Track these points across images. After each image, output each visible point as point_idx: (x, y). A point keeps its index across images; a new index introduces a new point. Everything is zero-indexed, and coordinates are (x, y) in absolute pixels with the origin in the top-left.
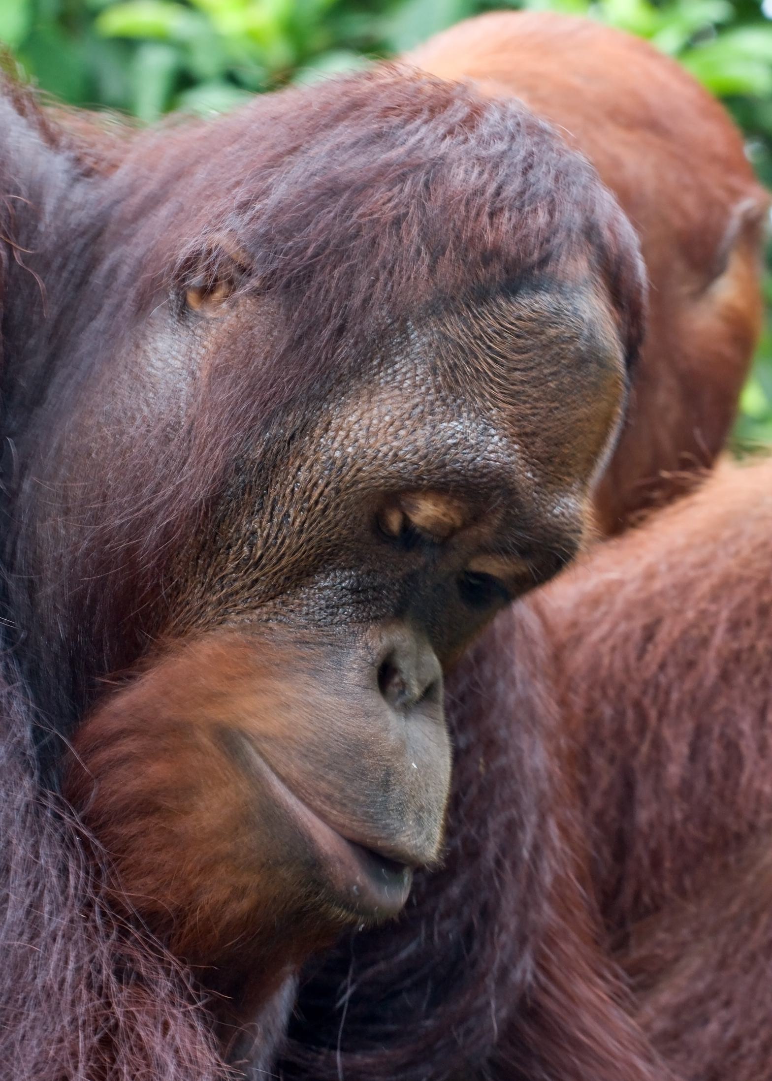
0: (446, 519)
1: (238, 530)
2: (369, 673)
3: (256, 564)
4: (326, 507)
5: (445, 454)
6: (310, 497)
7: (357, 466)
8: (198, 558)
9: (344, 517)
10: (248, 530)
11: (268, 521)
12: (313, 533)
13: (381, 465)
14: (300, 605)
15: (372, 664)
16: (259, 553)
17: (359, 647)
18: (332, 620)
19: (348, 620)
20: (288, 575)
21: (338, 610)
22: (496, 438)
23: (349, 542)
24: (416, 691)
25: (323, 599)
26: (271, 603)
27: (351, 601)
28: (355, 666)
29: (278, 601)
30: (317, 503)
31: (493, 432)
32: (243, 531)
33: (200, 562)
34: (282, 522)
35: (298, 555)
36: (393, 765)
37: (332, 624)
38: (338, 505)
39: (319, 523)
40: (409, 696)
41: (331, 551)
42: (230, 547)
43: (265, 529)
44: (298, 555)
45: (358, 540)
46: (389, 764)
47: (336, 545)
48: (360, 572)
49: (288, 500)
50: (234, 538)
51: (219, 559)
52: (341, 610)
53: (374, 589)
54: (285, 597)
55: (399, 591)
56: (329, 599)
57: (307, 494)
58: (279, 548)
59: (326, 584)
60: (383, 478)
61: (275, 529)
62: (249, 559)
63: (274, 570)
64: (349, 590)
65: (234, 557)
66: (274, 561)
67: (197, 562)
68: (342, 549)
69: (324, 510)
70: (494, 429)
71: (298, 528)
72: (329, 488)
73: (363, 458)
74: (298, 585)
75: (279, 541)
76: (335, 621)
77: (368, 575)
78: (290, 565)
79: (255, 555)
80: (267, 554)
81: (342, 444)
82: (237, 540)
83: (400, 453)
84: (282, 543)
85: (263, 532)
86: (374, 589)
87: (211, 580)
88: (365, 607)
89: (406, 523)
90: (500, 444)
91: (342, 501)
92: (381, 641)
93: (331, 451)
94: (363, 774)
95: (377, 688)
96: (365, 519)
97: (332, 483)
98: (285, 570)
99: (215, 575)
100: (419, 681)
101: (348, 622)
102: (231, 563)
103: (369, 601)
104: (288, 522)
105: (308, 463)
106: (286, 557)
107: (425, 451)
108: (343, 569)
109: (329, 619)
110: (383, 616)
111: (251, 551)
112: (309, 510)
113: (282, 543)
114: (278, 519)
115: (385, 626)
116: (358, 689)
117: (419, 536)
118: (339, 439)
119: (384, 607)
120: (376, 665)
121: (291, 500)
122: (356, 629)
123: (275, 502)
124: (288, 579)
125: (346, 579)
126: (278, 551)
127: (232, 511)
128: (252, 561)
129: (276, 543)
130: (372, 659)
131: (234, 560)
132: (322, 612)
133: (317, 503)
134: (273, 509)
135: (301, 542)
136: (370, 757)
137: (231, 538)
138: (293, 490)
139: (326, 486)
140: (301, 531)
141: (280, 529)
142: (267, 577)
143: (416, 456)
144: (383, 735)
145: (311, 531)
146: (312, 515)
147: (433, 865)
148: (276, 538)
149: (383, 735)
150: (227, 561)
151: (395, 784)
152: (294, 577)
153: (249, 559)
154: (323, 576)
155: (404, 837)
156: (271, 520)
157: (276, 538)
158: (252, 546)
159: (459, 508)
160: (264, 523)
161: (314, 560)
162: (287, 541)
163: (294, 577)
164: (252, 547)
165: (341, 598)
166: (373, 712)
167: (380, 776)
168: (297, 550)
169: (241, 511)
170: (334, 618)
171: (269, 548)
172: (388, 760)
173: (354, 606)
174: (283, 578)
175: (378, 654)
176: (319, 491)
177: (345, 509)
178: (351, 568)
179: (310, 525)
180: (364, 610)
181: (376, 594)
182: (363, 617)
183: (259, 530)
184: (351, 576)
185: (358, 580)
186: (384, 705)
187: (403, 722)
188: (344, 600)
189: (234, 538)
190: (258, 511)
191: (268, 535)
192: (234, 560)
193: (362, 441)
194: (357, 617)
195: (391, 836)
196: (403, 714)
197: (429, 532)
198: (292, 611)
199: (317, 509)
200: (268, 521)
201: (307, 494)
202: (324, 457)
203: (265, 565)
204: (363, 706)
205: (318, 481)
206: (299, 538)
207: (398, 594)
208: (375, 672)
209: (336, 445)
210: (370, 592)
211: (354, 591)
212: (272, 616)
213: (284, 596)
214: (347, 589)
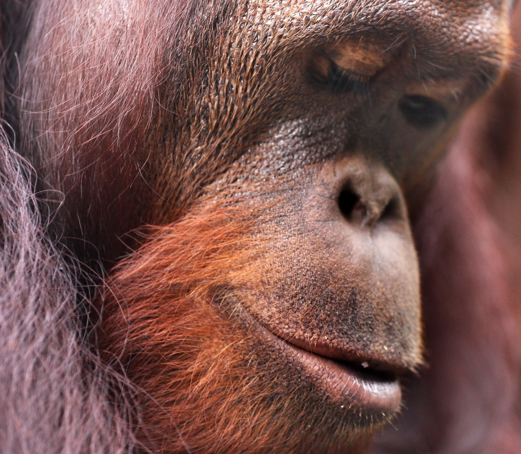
0: (367, 62)
1: (192, 108)
2: (328, 207)
3: (215, 132)
4: (261, 72)
5: (350, 11)
6: (245, 67)
7: (278, 34)
8: (164, 140)
9: (279, 76)
10: (200, 107)
11: (216, 95)
12: (256, 96)
13: (297, 30)
14: (261, 160)
15: (330, 197)
16: (215, 122)
17: (316, 185)
18: (290, 167)
19: (304, 163)
20: (245, 135)
21: (293, 157)
23: (289, 96)
24: (376, 210)
25: (279, 149)
26: (235, 164)
27: (303, 146)
28: (314, 204)
30: (252, 71)
32: (197, 108)
33: (167, 143)
34: (227, 93)
35: (248, 118)
36: (358, 286)
37: (290, 170)
38: (271, 68)
39: (259, 86)
40: (372, 216)
41: (276, 107)
42: (189, 123)
43: (214, 102)
44: (248, 118)
48: (307, 120)
49: (227, 73)
50: (191, 115)
51: (183, 137)
52: (296, 156)
53: (322, 131)
55: (345, 127)
56: (284, 148)
57: (242, 65)
58: (230, 115)
59: (280, 136)
60: (302, 39)
62: (207, 129)
63: (231, 135)
64: (300, 136)
65: (195, 131)
66: (229, 127)
67: (165, 144)
68: (285, 104)
71: (242, 95)
72: (259, 56)
73: (282, 27)
75: (229, 109)
76: (292, 166)
77: (314, 120)
78: (243, 127)
79: (211, 124)
80: (221, 122)
81: (262, 19)
82: (193, 116)
83: (311, 17)
84: (232, 109)
85: (213, 104)
86: (322, 131)
87: (180, 157)
88: (317, 149)
89: (334, 67)
91: (273, 64)
92: (335, 175)
93: (253, 27)
94: (332, 299)
96: (298, 74)
97: (261, 52)
98: (241, 131)
99: (183, 152)
100: (377, 201)
101: (304, 166)
102: (193, 137)
103: (320, 143)
104: (232, 92)
106: (238, 121)
107: (333, 12)
108: (292, 120)
109: (287, 166)
110: (334, 153)
111: (207, 122)
113: (232, 109)
114: (223, 90)
115: (336, 161)
117: (346, 78)
118: (258, 15)
119: (335, 145)
120: (333, 197)
121: (230, 72)
122: (311, 170)
123: (217, 77)
124: (245, 139)
125: (295, 128)
126: (230, 118)
127: (182, 93)
128: (210, 131)
129: (227, 110)
130: (329, 193)
131: (195, 133)
132: (280, 162)
133: (252, 71)
134: (217, 83)
135: (247, 106)
136: (336, 282)
137: (188, 116)
138: (229, 65)
139: (257, 55)
140: (245, 97)
142: (227, 142)
143: (325, 17)
145: (254, 95)
146: (251, 81)
147: (419, 367)
148: (226, 107)
150: (190, 136)
151: (362, 302)
152: (251, 136)
153: (207, 129)
154: (275, 129)
156: (218, 93)
157: (226, 107)
158: (206, 118)
160: (212, 97)
161: (263, 118)
162: (236, 108)
163: (251, 136)
164: (208, 119)
165: (295, 145)
166: (334, 242)
167: (346, 297)
168: (246, 113)
169: (190, 91)
170: (291, 164)
171: (221, 117)
172: (352, 282)
173: (307, 150)
174: (241, 139)
175: (334, 187)
176: (252, 60)
177: (277, 70)
178: (298, 118)
179: (252, 90)
180: (316, 152)
181: (325, 135)
182: (316, 158)
183: (210, 105)
184: (299, 125)
185: (306, 127)
188: (297, 146)
189: (191, 115)
190: (205, 88)
191: (219, 107)
192: (195, 133)
193: (278, 13)
194: (311, 159)
196: (369, 233)
197: (354, 73)
198: (255, 167)
199: (254, 75)
200: (216, 95)
201: (242, 65)
202: (249, 32)
203: (222, 131)
204: (324, 239)
205: (248, 53)
206: (245, 103)
208: (334, 203)
209: (257, 21)
210: (320, 134)
212: (238, 176)
213: (246, 155)
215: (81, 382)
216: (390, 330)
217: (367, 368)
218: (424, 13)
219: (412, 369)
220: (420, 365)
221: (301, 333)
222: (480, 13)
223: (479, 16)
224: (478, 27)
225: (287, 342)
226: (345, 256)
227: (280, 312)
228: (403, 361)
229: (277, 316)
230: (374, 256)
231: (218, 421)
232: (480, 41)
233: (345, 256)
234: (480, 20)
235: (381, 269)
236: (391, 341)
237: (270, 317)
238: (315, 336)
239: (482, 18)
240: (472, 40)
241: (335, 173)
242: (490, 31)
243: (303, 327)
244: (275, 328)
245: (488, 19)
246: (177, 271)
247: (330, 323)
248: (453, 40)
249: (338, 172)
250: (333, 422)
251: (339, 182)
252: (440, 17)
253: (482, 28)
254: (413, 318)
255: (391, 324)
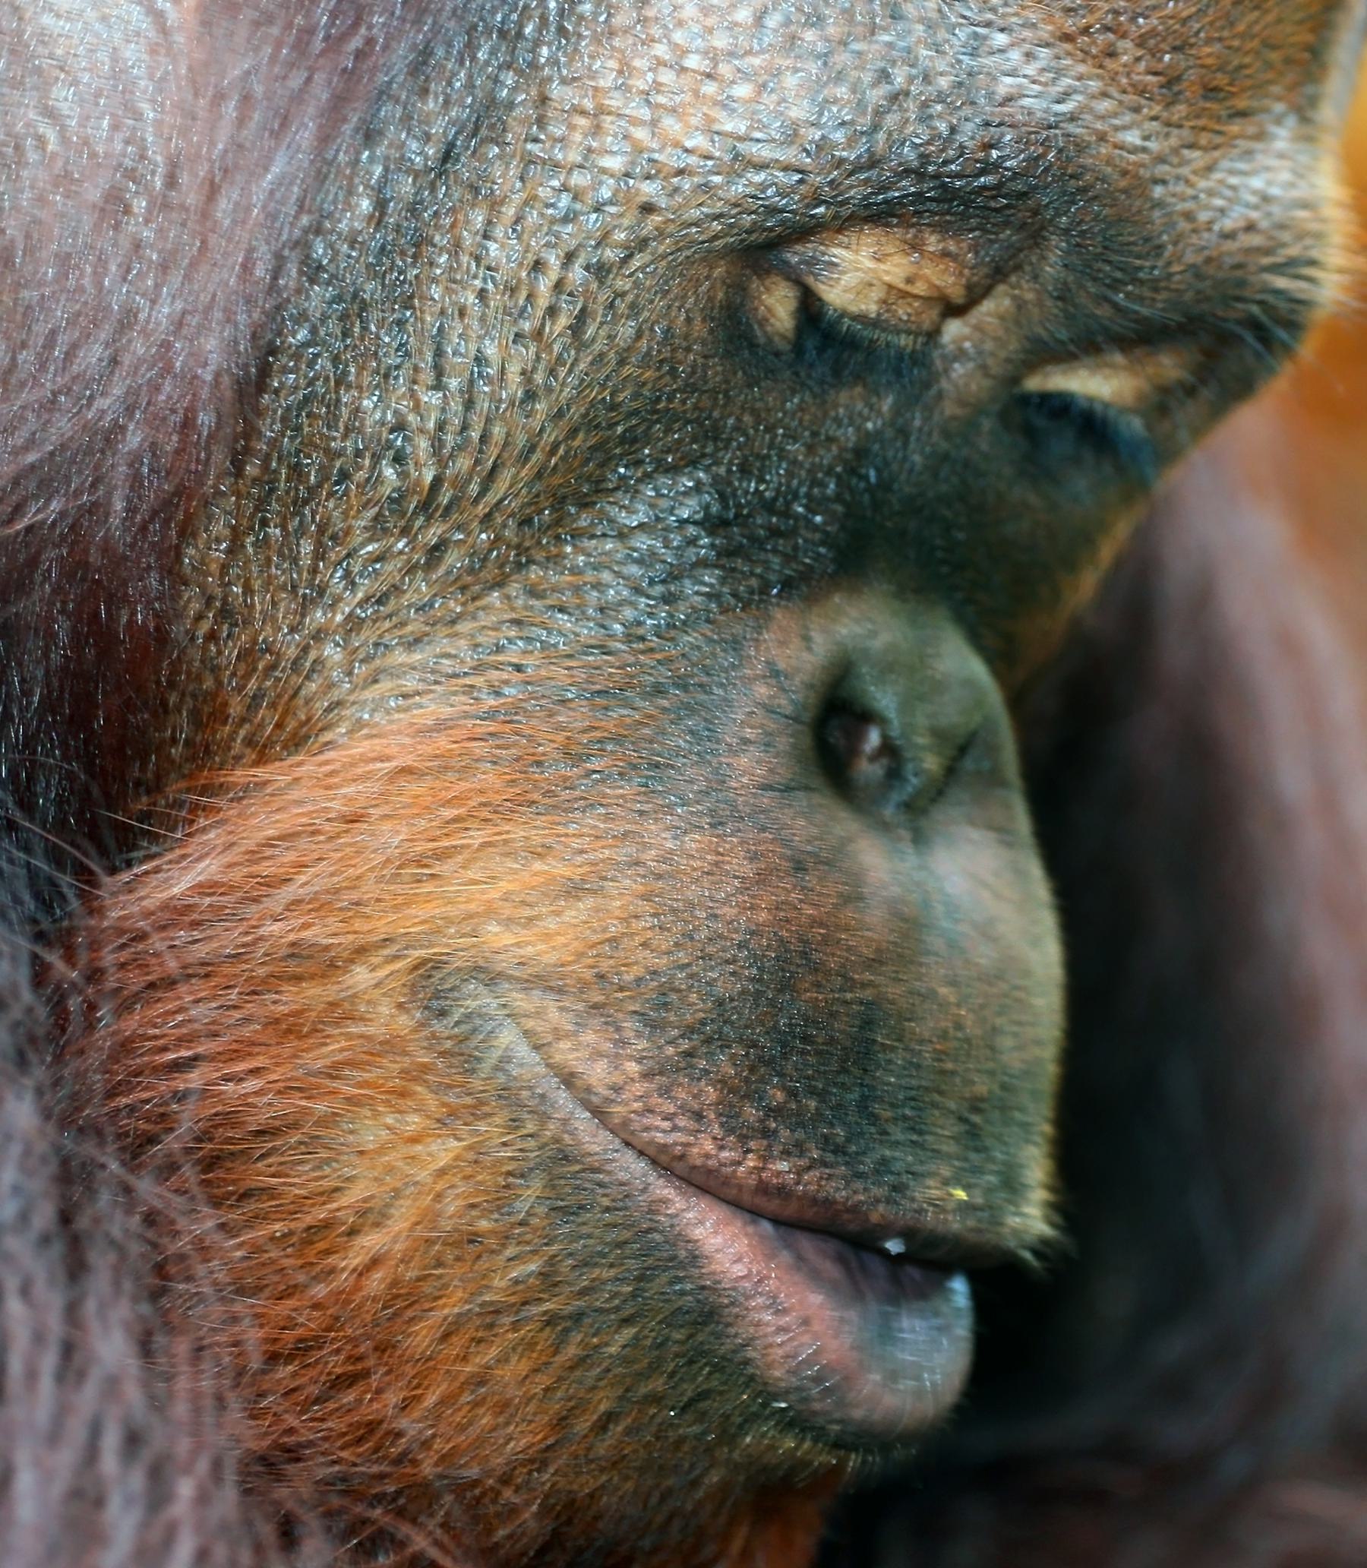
3: (426, 506)
4: (582, 317)
22: (1015, 55)
28: (749, 733)
29: (514, 588)
31: (1001, 39)
45: (689, 388)
46: (868, 994)
47: (635, 413)
54: (534, 573)
55: (838, 498)
61: (456, 406)
69: (577, 328)
70: (1002, 30)
74: (559, 528)
75: (475, 435)
84: (484, 438)
89: (810, 307)
90: (1031, 70)
92: (809, 649)
95: (817, 782)
96: (699, 328)
105: (510, 211)
108: (674, 470)
111: (403, 475)
112: (538, 334)
115: (812, 600)
116: (766, 800)
140: (530, 396)
141: (469, 404)
144: (848, 914)
147: (1042, 1249)
148: (465, 427)
149: (848, 914)
155: (1002, 1152)
156: (438, 386)
159: (945, 254)
168: (532, 449)
178: (694, 463)
186: (844, 823)
187: (910, 860)
191: (441, 426)
195: (868, 1220)
207: (839, 508)
211: (712, 524)
214: (695, 523)
215: (58, 1249)
216: (972, 1136)
217: (899, 1255)
218: (1102, 138)
219: (1027, 1255)
220: (1045, 1241)
221: (709, 1146)
222: (1261, 136)
223: (1258, 146)
224: (1257, 183)
225: (654, 1162)
226: (847, 900)
227: (646, 1076)
228: (1006, 1231)
229: (639, 1088)
230: (926, 904)
231: (276, 993)
232: (1264, 224)
233: (847, 900)
234: (1262, 160)
235: (952, 945)
236: (977, 1171)
237: (617, 1089)
238: (751, 1162)
239: (1264, 152)
240: (1242, 224)
241: (807, 639)
242: (1295, 194)
243: (716, 1130)
244: (626, 1123)
245: (1281, 156)
246: (320, 905)
247: (798, 1121)
248: (1183, 225)
249: (818, 637)
250: (412, 930)
251: (823, 667)
252: (1144, 150)
253: (1269, 183)
254: (1035, 1094)
255: (976, 1119)
